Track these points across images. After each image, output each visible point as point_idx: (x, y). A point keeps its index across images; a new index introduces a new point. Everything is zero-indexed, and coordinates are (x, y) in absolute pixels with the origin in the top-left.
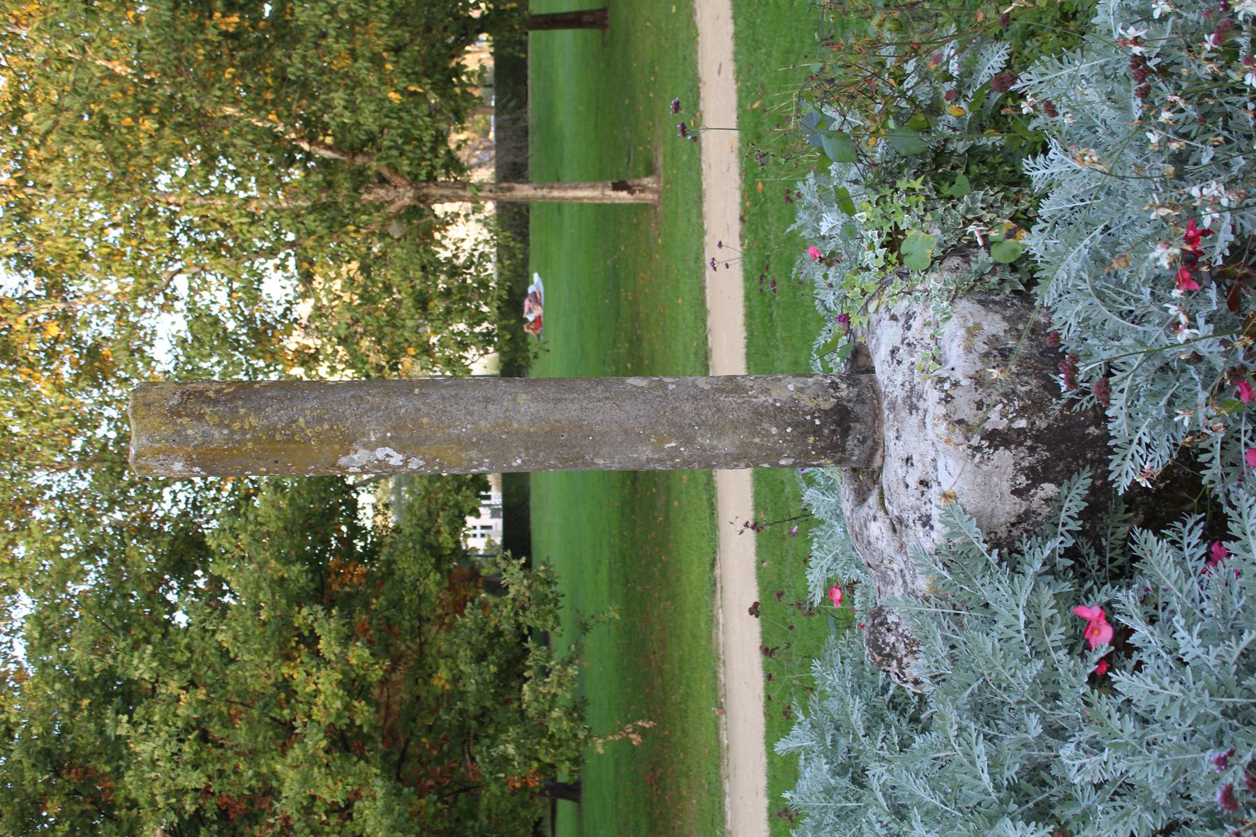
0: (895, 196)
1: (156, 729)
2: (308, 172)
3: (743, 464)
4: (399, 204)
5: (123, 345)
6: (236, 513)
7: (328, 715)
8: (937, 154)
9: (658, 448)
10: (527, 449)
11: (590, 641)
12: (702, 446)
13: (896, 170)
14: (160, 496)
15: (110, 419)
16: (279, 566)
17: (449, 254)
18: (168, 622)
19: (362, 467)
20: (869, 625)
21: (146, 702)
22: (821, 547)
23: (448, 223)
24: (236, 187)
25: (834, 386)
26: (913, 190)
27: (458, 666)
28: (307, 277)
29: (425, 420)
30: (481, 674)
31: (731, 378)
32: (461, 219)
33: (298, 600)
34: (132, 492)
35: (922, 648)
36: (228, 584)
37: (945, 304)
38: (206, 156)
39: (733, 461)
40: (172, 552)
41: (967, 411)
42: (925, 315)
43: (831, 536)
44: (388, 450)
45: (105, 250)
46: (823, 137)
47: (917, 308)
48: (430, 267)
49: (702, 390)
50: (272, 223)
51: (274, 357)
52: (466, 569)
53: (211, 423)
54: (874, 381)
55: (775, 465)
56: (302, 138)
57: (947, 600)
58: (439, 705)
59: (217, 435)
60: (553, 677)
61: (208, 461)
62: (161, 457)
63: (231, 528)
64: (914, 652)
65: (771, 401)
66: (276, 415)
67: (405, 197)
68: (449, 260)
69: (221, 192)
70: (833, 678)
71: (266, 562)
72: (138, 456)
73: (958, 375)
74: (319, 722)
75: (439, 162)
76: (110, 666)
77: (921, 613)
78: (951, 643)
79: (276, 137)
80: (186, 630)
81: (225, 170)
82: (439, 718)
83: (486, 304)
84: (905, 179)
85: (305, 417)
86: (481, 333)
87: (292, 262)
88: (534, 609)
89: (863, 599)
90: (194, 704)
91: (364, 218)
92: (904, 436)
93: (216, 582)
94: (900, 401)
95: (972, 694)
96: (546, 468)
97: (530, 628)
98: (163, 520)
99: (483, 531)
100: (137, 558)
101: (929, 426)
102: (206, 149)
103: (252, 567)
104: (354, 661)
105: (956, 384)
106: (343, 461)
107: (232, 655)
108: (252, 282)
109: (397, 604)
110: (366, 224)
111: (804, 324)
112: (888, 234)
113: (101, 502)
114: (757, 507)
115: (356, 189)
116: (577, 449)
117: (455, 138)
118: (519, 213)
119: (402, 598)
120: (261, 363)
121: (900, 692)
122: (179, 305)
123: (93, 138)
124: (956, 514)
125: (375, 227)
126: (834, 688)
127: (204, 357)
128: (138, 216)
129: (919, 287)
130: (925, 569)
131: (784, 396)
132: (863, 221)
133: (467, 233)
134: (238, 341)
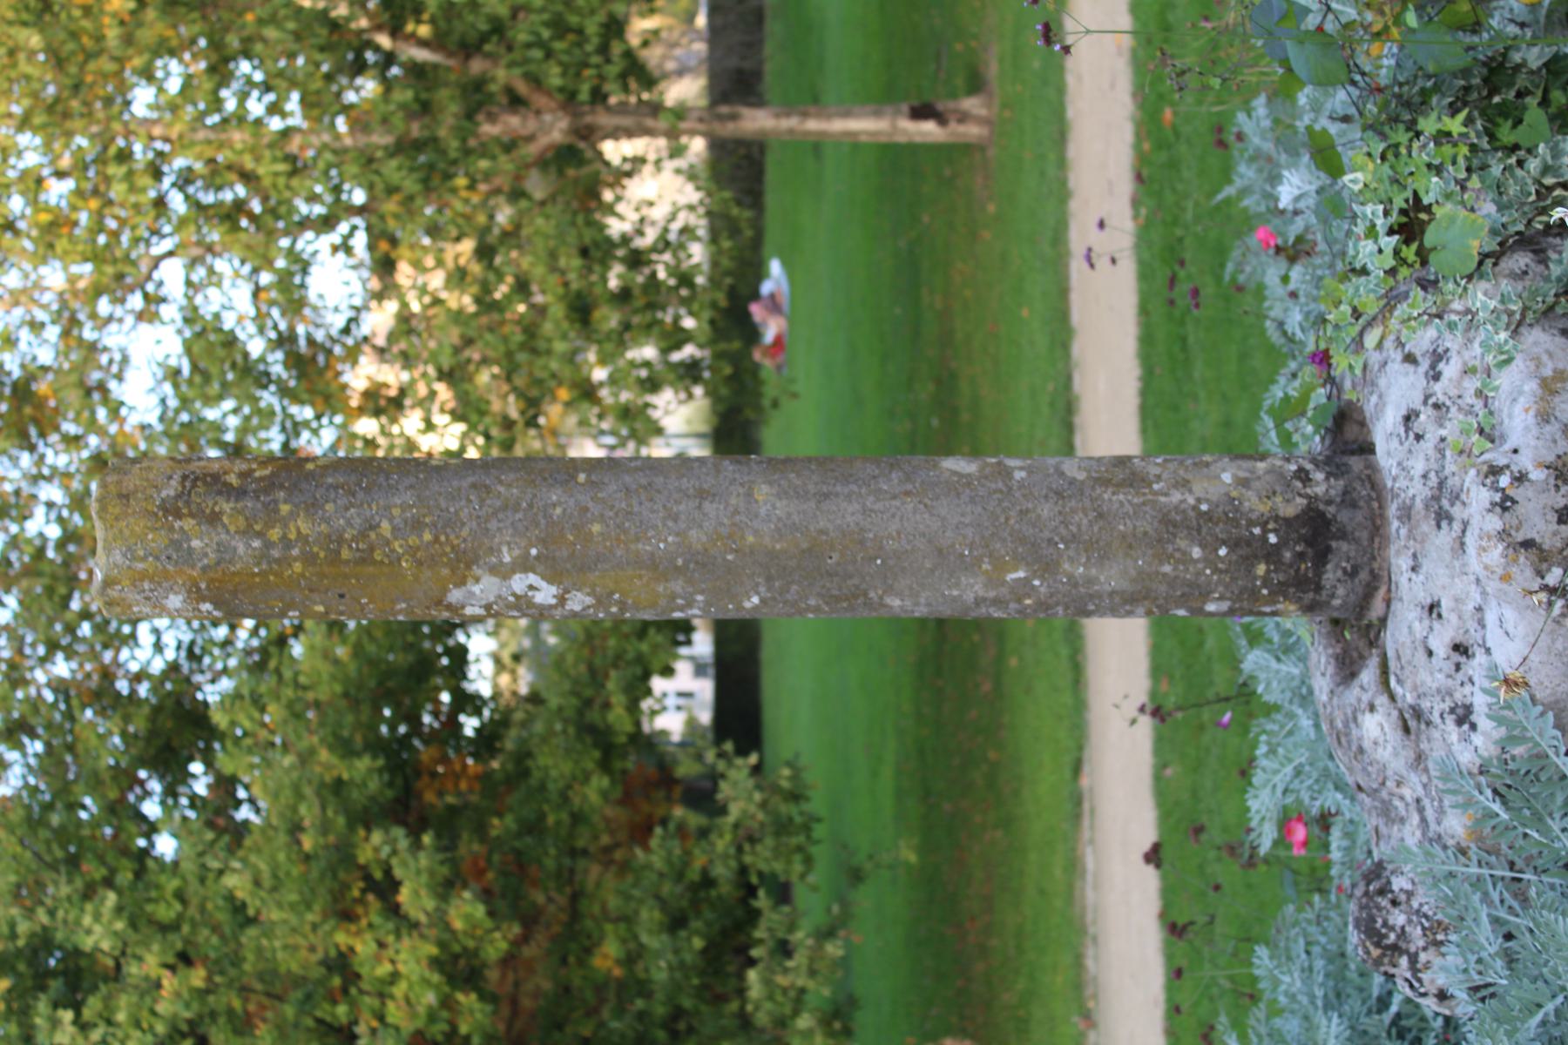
0: (1416, 145)
1: (120, 1034)
2: (388, 85)
3: (1141, 610)
4: (544, 141)
5: (73, 378)
6: (259, 668)
7: (413, 1015)
8: (1492, 71)
9: (994, 581)
10: (769, 579)
11: (864, 898)
12: (1070, 577)
13: (1417, 99)
14: (133, 636)
15: (50, 505)
16: (334, 760)
17: (626, 227)
18: (145, 853)
19: (488, 607)
20: (1359, 892)
21: (103, 988)
22: (1272, 751)
23: (629, 174)
24: (260, 104)
25: (1303, 476)
26: (1449, 134)
27: (636, 937)
28: (385, 266)
29: (596, 528)
30: (676, 952)
31: (1122, 461)
32: (648, 169)
33: (365, 818)
34: (85, 629)
35: (1453, 937)
36: (247, 787)
37: (1503, 336)
38: (214, 57)
39: (1122, 604)
40: (153, 733)
41: (1541, 526)
42: (1467, 355)
43: (1290, 733)
44: (532, 579)
45: (44, 218)
46: (1289, 44)
47: (1452, 342)
48: (597, 251)
49: (1072, 482)
50: (326, 173)
51: (329, 398)
52: (651, 770)
53: (232, 529)
54: (1373, 468)
55: (1200, 611)
56: (379, 28)
57: (1496, 852)
58: (602, 1001)
59: (241, 549)
60: (799, 960)
61: (224, 595)
62: (146, 586)
63: (252, 693)
64: (1438, 944)
65: (1191, 501)
66: (342, 517)
67: (555, 129)
68: (625, 239)
69: (240, 117)
70: (1291, 980)
71: (312, 752)
72: (108, 583)
73: (1525, 462)
74: (397, 1029)
75: (613, 70)
76: (44, 928)
77: (1451, 875)
78: (1505, 930)
79: (335, 26)
80: (176, 864)
81: (249, 82)
82: (602, 1025)
83: (691, 313)
84: (1434, 115)
85: (391, 519)
86: (682, 364)
87: (360, 241)
88: (769, 841)
89: (1345, 843)
90: (186, 995)
91: (484, 164)
92: (1426, 565)
93: (225, 785)
94: (1419, 504)
95: (1543, 1023)
96: (801, 612)
97: (760, 874)
98: (138, 678)
99: (680, 701)
100: (94, 741)
101: (1471, 548)
102: (216, 45)
103: (288, 760)
104: (458, 925)
105: (1521, 478)
106: (455, 596)
107: (251, 912)
108: (291, 274)
109: (533, 827)
110: (487, 177)
111: (1243, 357)
112: (1403, 212)
113: (33, 645)
114: (1158, 670)
115: (470, 115)
116: (856, 581)
117: (640, 25)
118: (748, 157)
119: (542, 817)
120: (308, 413)
121: (1408, 1009)
122: (167, 311)
123: (25, 24)
124: (1517, 705)
125: (503, 181)
126: (1293, 998)
127: (211, 401)
128: (101, 160)
129: (1457, 305)
130: (1460, 799)
131: (1215, 492)
132: (1357, 188)
133: (657, 192)
134: (268, 374)
